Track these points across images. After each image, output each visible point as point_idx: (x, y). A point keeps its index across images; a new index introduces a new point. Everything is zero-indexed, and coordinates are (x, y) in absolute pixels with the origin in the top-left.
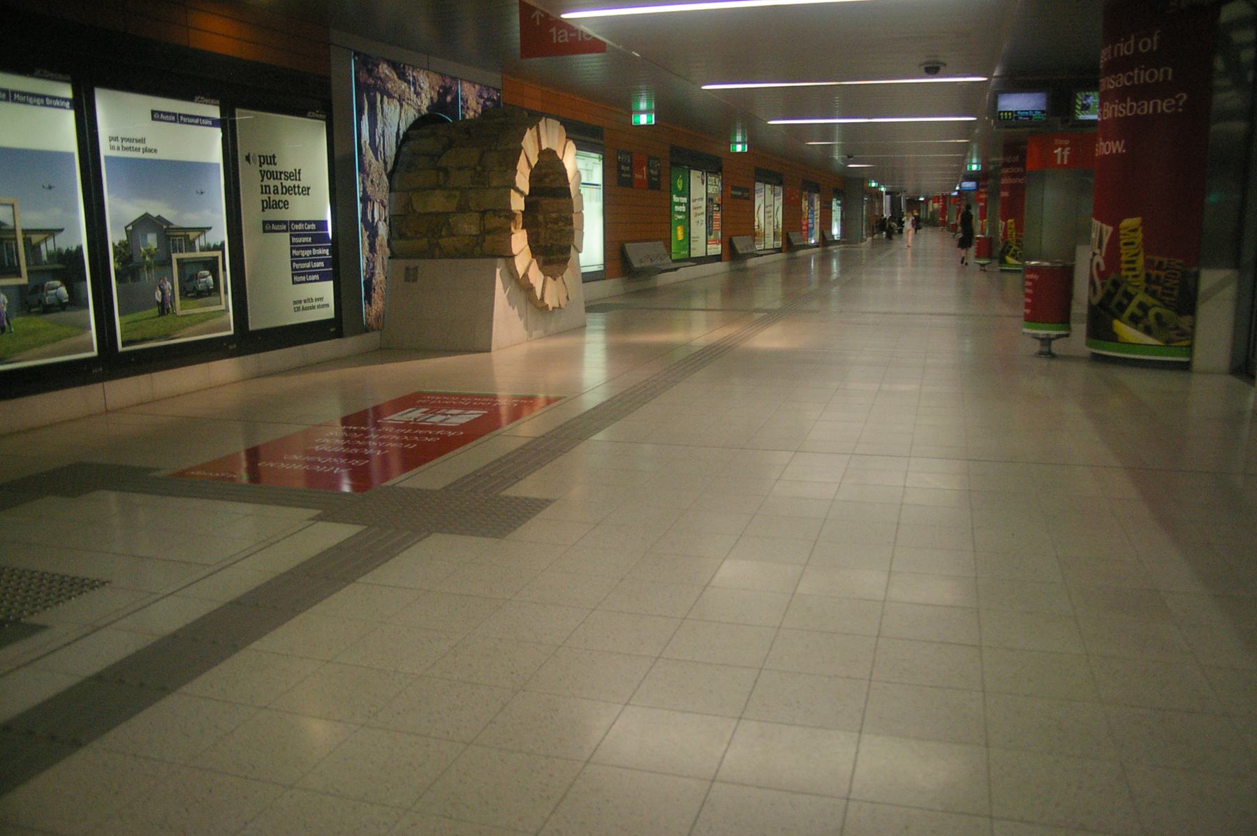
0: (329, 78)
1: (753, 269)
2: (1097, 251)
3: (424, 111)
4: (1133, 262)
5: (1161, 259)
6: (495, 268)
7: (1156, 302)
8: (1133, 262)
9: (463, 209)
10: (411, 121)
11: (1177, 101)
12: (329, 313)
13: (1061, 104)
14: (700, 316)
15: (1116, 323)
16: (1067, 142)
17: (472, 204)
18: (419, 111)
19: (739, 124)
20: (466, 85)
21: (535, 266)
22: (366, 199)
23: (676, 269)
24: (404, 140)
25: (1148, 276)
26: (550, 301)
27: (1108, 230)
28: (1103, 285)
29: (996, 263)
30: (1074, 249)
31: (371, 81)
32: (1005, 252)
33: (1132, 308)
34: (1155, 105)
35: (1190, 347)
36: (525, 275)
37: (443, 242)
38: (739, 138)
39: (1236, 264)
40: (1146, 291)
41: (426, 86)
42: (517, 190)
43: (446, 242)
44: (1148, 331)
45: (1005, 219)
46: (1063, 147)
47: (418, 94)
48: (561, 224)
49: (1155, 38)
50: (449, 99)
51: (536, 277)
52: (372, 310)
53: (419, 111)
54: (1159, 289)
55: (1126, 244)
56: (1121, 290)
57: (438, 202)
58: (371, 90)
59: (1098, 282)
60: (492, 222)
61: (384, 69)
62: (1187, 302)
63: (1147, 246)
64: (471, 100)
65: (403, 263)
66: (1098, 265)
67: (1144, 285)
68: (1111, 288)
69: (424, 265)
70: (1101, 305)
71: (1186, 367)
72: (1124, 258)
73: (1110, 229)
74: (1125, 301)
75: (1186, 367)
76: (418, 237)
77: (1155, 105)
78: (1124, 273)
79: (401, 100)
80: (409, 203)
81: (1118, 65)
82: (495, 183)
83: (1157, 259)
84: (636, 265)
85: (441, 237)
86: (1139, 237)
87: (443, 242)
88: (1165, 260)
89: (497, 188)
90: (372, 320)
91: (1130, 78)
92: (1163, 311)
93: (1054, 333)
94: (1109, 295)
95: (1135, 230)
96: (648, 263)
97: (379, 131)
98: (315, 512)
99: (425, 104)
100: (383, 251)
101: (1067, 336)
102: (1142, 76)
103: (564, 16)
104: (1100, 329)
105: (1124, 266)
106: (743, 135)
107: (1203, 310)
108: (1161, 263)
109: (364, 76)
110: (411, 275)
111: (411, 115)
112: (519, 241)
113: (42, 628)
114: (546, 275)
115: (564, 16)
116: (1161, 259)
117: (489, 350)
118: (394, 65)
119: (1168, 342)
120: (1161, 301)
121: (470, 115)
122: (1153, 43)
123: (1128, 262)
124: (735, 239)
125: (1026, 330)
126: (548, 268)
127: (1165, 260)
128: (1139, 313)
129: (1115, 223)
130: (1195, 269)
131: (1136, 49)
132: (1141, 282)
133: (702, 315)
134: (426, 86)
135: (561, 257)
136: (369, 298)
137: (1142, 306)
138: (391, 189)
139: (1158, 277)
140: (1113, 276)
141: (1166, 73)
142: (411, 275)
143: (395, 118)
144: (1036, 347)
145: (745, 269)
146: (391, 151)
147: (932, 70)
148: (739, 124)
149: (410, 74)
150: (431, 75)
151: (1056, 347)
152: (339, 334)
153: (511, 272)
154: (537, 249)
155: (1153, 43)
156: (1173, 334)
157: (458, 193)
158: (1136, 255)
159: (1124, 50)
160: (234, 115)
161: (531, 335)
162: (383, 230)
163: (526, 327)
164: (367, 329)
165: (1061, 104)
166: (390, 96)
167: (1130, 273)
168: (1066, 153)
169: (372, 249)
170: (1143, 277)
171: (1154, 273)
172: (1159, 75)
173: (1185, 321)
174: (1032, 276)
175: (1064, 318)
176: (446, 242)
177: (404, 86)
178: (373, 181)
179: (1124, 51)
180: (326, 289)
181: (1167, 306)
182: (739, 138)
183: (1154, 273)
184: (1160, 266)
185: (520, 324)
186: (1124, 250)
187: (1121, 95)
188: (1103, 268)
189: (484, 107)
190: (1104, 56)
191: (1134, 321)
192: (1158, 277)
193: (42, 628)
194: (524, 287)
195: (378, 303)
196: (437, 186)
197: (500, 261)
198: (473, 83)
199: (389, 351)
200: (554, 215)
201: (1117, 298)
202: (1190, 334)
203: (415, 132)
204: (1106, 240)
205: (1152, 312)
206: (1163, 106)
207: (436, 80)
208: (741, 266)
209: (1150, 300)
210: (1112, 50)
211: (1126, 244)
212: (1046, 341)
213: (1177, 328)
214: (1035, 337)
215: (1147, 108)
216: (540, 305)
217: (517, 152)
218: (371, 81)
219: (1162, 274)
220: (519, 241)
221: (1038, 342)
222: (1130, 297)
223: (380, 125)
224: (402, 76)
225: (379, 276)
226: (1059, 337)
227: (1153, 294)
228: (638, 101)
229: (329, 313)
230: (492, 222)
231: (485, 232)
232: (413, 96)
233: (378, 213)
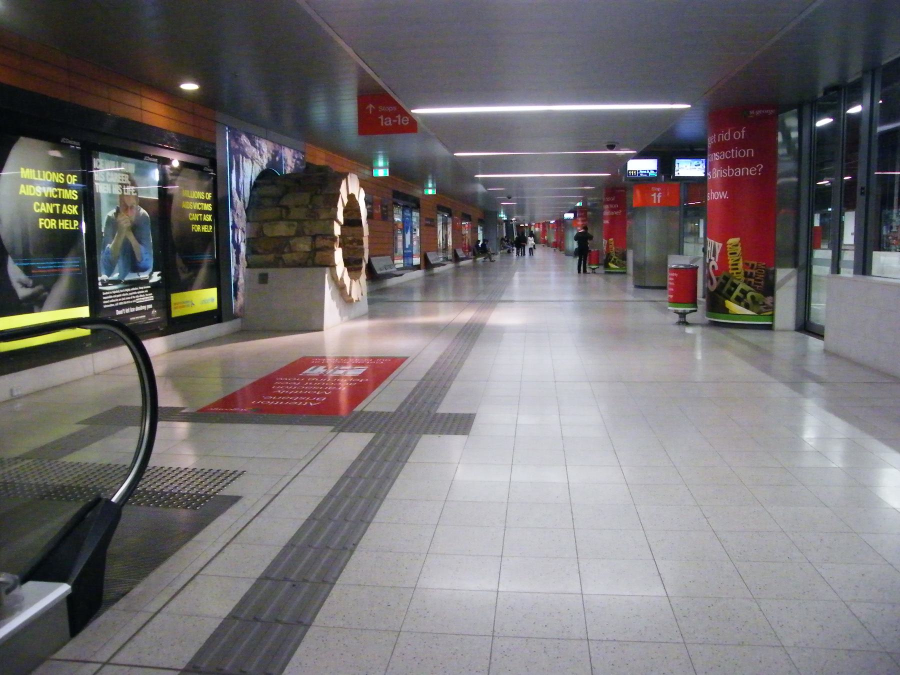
0: (214, 144)
1: (437, 274)
2: (713, 258)
3: (265, 167)
4: (736, 265)
5: (753, 262)
8: (736, 265)
9: (300, 234)
11: (758, 168)
13: (666, 167)
16: (659, 190)
17: (307, 231)
18: (262, 167)
21: (346, 273)
22: (234, 227)
23: (401, 275)
24: (254, 186)
25: (746, 273)
27: (719, 246)
28: (717, 279)
29: (602, 267)
30: (667, 259)
33: (737, 293)
34: (745, 171)
35: (772, 315)
40: (745, 282)
42: (338, 222)
44: (747, 306)
45: (607, 239)
46: (657, 193)
47: (261, 155)
49: (743, 131)
50: (277, 159)
51: (347, 280)
52: (237, 304)
53: (262, 167)
54: (753, 280)
56: (729, 282)
57: (282, 229)
58: (238, 152)
59: (714, 277)
60: (320, 243)
61: (244, 139)
63: (745, 255)
65: (257, 271)
66: (713, 267)
67: (743, 279)
69: (270, 271)
71: (770, 328)
72: (730, 262)
73: (721, 245)
76: (268, 253)
77: (745, 171)
78: (731, 272)
79: (252, 160)
80: (261, 229)
81: (720, 147)
83: (751, 263)
85: (283, 253)
88: (755, 263)
89: (324, 220)
90: (237, 311)
91: (729, 154)
93: (688, 309)
94: (722, 286)
95: (737, 245)
96: (384, 271)
97: (241, 180)
100: (243, 263)
102: (735, 153)
103: (413, 111)
104: (716, 304)
105: (730, 267)
108: (753, 265)
109: (233, 143)
110: (264, 279)
111: (257, 170)
112: (338, 255)
113: (235, 499)
114: (351, 278)
115: (413, 111)
116: (753, 262)
117: (321, 330)
118: (249, 136)
119: (759, 313)
122: (742, 134)
124: (428, 254)
125: (670, 308)
126: (353, 273)
127: (755, 263)
128: (741, 295)
129: (724, 242)
130: (772, 269)
131: (732, 137)
132: (741, 277)
133: (442, 304)
134: (265, 150)
135: (356, 266)
136: (236, 295)
137: (742, 291)
138: (248, 221)
140: (724, 273)
141: (750, 152)
143: (250, 171)
144: (677, 318)
145: (433, 275)
146: (247, 194)
147: (611, 147)
148: (430, 177)
151: (689, 318)
152: (219, 320)
153: (334, 277)
154: (347, 262)
155: (742, 134)
156: (762, 308)
157: (295, 223)
159: (725, 137)
163: (340, 314)
164: (235, 317)
165: (666, 167)
166: (247, 157)
167: (735, 272)
168: (659, 196)
169: (238, 262)
170: (743, 273)
171: (749, 271)
172: (746, 153)
173: (768, 300)
175: (694, 302)
176: (287, 257)
177: (254, 150)
178: (238, 216)
179: (724, 138)
180: (213, 293)
181: (758, 291)
183: (749, 271)
185: (337, 311)
186: (730, 257)
187: (724, 164)
188: (717, 268)
190: (710, 141)
191: (738, 301)
192: (751, 273)
193: (235, 499)
194: (340, 288)
195: (241, 299)
197: (327, 269)
198: (290, 148)
199: (247, 332)
200: (350, 238)
201: (728, 286)
202: (772, 308)
203: (261, 182)
204: (718, 252)
205: (749, 295)
206: (750, 172)
207: (271, 144)
208: (431, 272)
209: (747, 288)
210: (717, 137)
212: (683, 315)
213: (764, 304)
214: (676, 312)
215: (740, 172)
217: (337, 195)
218: (237, 147)
219: (754, 271)
220: (338, 255)
222: (735, 286)
225: (241, 281)
226: (691, 312)
227: (749, 284)
228: (377, 159)
229: (213, 305)
230: (320, 243)
231: (315, 250)
233: (241, 237)
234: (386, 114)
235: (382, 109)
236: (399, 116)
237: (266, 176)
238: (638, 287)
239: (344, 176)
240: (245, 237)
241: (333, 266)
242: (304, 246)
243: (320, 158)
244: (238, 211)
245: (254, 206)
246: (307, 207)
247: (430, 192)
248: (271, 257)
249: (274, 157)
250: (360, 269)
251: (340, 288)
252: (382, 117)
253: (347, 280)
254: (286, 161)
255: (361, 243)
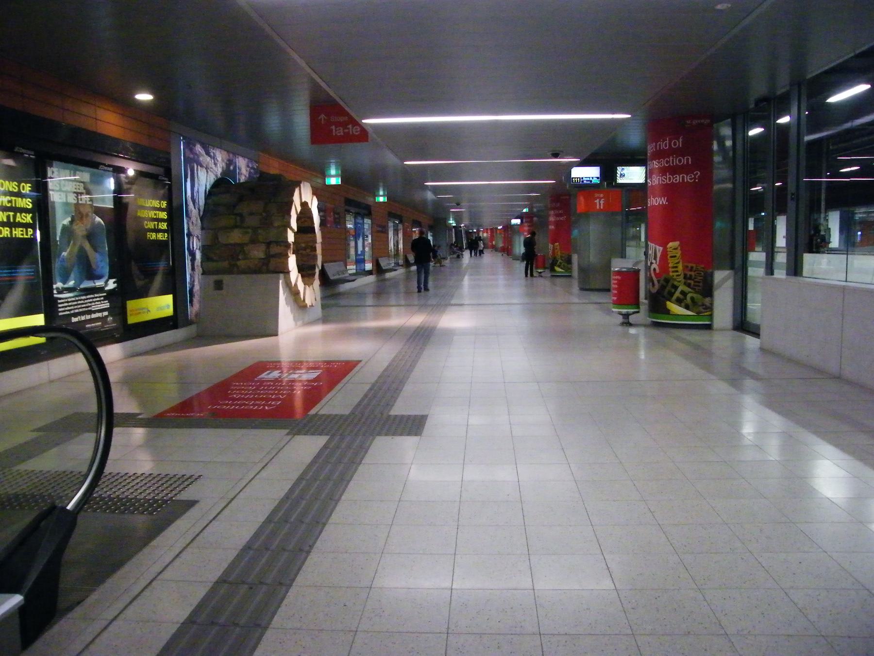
0: (169, 153)
2: (654, 261)
3: (219, 176)
6: (278, 279)
7: (690, 290)
9: (254, 241)
10: (212, 181)
11: (695, 175)
12: (169, 311)
13: (608, 175)
14: (394, 309)
15: (668, 303)
16: (602, 195)
17: (261, 238)
18: (216, 176)
19: (381, 184)
20: (241, 159)
22: (189, 235)
23: (354, 281)
25: (685, 275)
26: (308, 302)
27: (659, 249)
29: (547, 271)
31: (192, 156)
32: (554, 264)
33: (677, 294)
34: (683, 177)
35: (711, 317)
36: (296, 285)
37: (239, 263)
38: (381, 193)
39: (732, 268)
40: (685, 284)
41: (220, 159)
43: (242, 263)
44: (687, 307)
45: (553, 243)
46: (600, 199)
47: (215, 164)
48: (308, 251)
50: (232, 168)
51: (301, 286)
52: (193, 310)
54: (692, 282)
55: (672, 257)
56: (670, 284)
57: (236, 237)
58: (192, 161)
60: (275, 249)
61: (198, 148)
62: (708, 290)
64: (243, 168)
67: (683, 280)
68: (665, 284)
69: (226, 279)
70: (658, 292)
71: (709, 327)
72: (671, 265)
73: (661, 248)
74: (673, 290)
75: (709, 327)
77: (683, 177)
78: (671, 274)
79: (207, 168)
80: (216, 237)
81: (659, 155)
82: (276, 224)
83: (690, 265)
84: (332, 278)
86: (678, 253)
87: (239, 263)
88: (694, 265)
91: (667, 162)
92: (695, 295)
94: (663, 287)
97: (196, 189)
98: (288, 431)
99: (219, 171)
100: (199, 270)
101: (638, 312)
102: (674, 161)
103: (364, 121)
104: (657, 305)
105: (671, 270)
106: (384, 190)
107: (717, 294)
108: (692, 267)
110: (219, 285)
111: (212, 179)
112: (292, 261)
113: (191, 504)
115: (364, 121)
119: (698, 313)
120: (694, 289)
121: (243, 179)
122: (679, 143)
123: (673, 267)
124: (380, 259)
126: (306, 279)
128: (681, 297)
132: (681, 278)
134: (220, 159)
136: (191, 301)
137: (683, 293)
138: (203, 228)
139: (691, 276)
140: (664, 276)
141: (688, 159)
142: (219, 285)
143: (205, 180)
144: (620, 319)
145: (385, 280)
146: (202, 201)
147: (556, 155)
148: (381, 184)
149: (212, 151)
150: (223, 152)
151: (632, 319)
152: (175, 326)
153: (288, 283)
154: (301, 269)
155: (679, 143)
157: (250, 230)
158: (678, 263)
160: (45, 176)
161: (296, 325)
162: (198, 255)
163: (295, 319)
166: (202, 166)
167: (675, 274)
168: (602, 202)
169: (193, 269)
170: (682, 276)
171: (689, 273)
172: (684, 161)
173: (707, 301)
174: (617, 277)
175: (636, 303)
176: (242, 263)
177: (208, 159)
178: (193, 224)
179: (663, 146)
181: (696, 292)
182: (381, 193)
183: (689, 273)
184: (691, 270)
185: (291, 317)
187: (663, 171)
188: (658, 271)
189: (250, 173)
190: (650, 149)
191: (679, 302)
194: (294, 293)
195: (197, 306)
196: (236, 227)
197: (282, 276)
199: (203, 338)
201: (668, 288)
202: (710, 308)
203: (214, 190)
204: (659, 255)
205: (689, 296)
206: (688, 179)
209: (686, 289)
211: (672, 257)
212: (626, 316)
213: (703, 305)
214: (620, 313)
215: (678, 178)
216: (302, 304)
217: (291, 203)
218: (192, 156)
219: (693, 273)
220: (292, 261)
221: (621, 317)
222: (676, 288)
223: (196, 185)
224: (208, 154)
225: (197, 288)
226: (634, 313)
227: (689, 286)
228: (329, 168)
229: (169, 311)
230: (275, 249)
231: (269, 257)
232: (213, 166)
233: (196, 244)
234: (338, 124)
235: (333, 119)
236: (350, 126)
237: (220, 185)
238: (582, 289)
239: (298, 184)
240: (200, 244)
241: (287, 272)
242: (258, 253)
243: (274, 167)
244: (194, 219)
245: (209, 214)
246: (261, 214)
247: (381, 199)
248: (225, 264)
249: (228, 165)
250: (314, 275)
251: (294, 293)
252: (333, 127)
253: (301, 286)
254: (240, 169)
255: (315, 249)
